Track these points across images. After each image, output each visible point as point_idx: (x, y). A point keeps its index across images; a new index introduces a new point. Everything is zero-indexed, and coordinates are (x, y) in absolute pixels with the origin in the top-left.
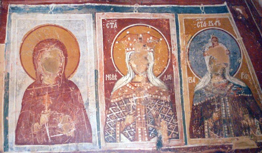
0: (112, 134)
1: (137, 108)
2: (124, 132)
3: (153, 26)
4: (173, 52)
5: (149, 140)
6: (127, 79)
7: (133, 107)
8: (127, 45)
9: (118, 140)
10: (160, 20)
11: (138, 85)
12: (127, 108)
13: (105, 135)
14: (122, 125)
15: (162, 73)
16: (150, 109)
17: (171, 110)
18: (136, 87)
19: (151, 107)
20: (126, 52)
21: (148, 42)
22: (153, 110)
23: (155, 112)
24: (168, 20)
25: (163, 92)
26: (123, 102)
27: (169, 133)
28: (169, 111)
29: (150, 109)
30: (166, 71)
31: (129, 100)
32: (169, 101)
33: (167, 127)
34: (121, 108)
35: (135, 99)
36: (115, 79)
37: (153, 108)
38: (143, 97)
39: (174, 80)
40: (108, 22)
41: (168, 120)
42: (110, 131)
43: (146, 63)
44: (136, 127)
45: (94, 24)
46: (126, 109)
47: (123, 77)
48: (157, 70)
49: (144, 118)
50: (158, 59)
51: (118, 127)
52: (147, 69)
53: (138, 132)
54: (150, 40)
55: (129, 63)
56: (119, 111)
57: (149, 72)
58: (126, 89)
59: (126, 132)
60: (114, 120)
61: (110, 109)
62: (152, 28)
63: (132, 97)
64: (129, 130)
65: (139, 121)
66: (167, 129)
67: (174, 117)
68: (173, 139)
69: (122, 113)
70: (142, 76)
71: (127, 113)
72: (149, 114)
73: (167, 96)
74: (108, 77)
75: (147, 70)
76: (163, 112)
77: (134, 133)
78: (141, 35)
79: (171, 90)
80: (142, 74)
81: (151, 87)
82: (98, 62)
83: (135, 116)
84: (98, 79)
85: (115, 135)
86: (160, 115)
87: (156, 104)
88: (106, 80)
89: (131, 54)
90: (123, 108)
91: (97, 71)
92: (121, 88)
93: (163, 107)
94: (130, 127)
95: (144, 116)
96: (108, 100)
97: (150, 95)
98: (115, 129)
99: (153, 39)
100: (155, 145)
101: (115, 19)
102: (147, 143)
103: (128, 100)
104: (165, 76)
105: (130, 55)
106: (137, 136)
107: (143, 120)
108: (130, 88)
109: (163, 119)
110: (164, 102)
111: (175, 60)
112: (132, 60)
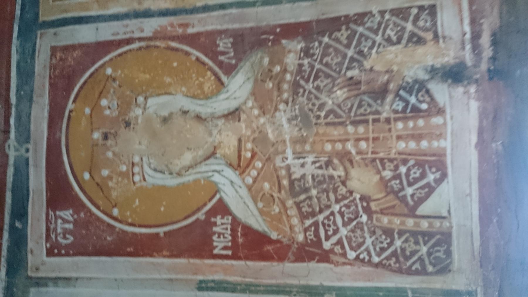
0: (418, 248)
1: (323, 152)
2: (411, 203)
3: (69, 97)
4: (148, 33)
5: (441, 112)
6: (228, 183)
7: (320, 167)
8: (123, 179)
9: (441, 226)
10: (52, 76)
11: (249, 146)
12: (325, 186)
13: (423, 272)
14: (387, 208)
15: (211, 69)
16: (327, 108)
17: (333, 36)
18: (254, 155)
19: (321, 107)
20: (144, 184)
21: (115, 114)
22: (332, 99)
23: (339, 92)
24: (54, 50)
25: (272, 63)
26: (304, 200)
27: (415, 39)
28: (337, 40)
29: (327, 108)
30: (206, 55)
31: (295, 179)
32: (302, 45)
33: (393, 48)
34: (322, 207)
35: (294, 159)
36: (230, 221)
37: (324, 98)
38: (287, 130)
39: (234, 30)
40: (56, 237)
41: (369, 43)
42: (408, 253)
43: (179, 121)
44: (392, 156)
45: (60, 283)
46: (326, 191)
47: (222, 194)
48: (201, 86)
49: (361, 129)
50: (168, 80)
51: (390, 222)
52: (198, 118)
53: (408, 151)
54: (109, 108)
55: (179, 174)
56: (332, 214)
57: (209, 110)
58: (262, 189)
59: (412, 196)
60: (367, 235)
61: (327, 245)
62: (74, 101)
63: (288, 168)
64: (405, 182)
65: (371, 145)
66: (400, 47)
67: (359, 25)
68: (435, 24)
69: (342, 204)
70: (220, 132)
71: (341, 187)
72: (344, 111)
73: (285, 52)
74: (221, 245)
75: (203, 116)
76: (341, 64)
77: (414, 166)
78: (96, 135)
79: (265, 40)
80: (215, 132)
81: (255, 104)
82: (173, 276)
83: (351, 162)
84: (228, 283)
85: (424, 234)
86: (349, 74)
87: (310, 86)
88: (230, 253)
89: (152, 166)
90: (324, 201)
91: (201, 282)
92: (255, 202)
93: (321, 62)
94: (394, 178)
95: (350, 129)
96: (295, 250)
97: (282, 106)
98: (401, 233)
99: (106, 98)
100: (460, 90)
101: (47, 214)
102: (452, 118)
103: (296, 183)
104: (221, 58)
105: (155, 170)
106: (425, 155)
107: (367, 131)
108: (258, 174)
109: (365, 63)
110: (306, 62)
111: (172, 25)
112: (170, 166)
